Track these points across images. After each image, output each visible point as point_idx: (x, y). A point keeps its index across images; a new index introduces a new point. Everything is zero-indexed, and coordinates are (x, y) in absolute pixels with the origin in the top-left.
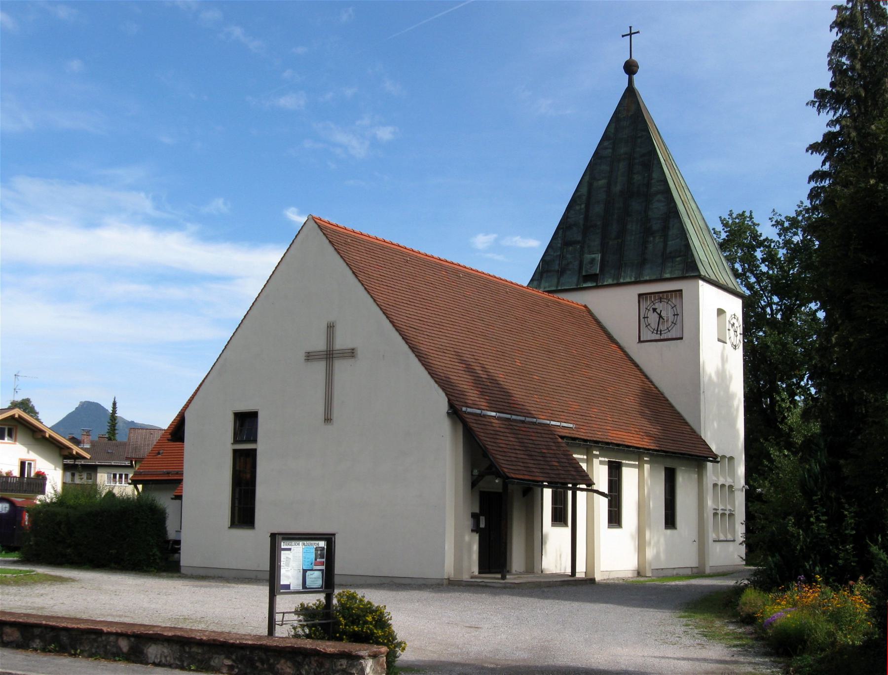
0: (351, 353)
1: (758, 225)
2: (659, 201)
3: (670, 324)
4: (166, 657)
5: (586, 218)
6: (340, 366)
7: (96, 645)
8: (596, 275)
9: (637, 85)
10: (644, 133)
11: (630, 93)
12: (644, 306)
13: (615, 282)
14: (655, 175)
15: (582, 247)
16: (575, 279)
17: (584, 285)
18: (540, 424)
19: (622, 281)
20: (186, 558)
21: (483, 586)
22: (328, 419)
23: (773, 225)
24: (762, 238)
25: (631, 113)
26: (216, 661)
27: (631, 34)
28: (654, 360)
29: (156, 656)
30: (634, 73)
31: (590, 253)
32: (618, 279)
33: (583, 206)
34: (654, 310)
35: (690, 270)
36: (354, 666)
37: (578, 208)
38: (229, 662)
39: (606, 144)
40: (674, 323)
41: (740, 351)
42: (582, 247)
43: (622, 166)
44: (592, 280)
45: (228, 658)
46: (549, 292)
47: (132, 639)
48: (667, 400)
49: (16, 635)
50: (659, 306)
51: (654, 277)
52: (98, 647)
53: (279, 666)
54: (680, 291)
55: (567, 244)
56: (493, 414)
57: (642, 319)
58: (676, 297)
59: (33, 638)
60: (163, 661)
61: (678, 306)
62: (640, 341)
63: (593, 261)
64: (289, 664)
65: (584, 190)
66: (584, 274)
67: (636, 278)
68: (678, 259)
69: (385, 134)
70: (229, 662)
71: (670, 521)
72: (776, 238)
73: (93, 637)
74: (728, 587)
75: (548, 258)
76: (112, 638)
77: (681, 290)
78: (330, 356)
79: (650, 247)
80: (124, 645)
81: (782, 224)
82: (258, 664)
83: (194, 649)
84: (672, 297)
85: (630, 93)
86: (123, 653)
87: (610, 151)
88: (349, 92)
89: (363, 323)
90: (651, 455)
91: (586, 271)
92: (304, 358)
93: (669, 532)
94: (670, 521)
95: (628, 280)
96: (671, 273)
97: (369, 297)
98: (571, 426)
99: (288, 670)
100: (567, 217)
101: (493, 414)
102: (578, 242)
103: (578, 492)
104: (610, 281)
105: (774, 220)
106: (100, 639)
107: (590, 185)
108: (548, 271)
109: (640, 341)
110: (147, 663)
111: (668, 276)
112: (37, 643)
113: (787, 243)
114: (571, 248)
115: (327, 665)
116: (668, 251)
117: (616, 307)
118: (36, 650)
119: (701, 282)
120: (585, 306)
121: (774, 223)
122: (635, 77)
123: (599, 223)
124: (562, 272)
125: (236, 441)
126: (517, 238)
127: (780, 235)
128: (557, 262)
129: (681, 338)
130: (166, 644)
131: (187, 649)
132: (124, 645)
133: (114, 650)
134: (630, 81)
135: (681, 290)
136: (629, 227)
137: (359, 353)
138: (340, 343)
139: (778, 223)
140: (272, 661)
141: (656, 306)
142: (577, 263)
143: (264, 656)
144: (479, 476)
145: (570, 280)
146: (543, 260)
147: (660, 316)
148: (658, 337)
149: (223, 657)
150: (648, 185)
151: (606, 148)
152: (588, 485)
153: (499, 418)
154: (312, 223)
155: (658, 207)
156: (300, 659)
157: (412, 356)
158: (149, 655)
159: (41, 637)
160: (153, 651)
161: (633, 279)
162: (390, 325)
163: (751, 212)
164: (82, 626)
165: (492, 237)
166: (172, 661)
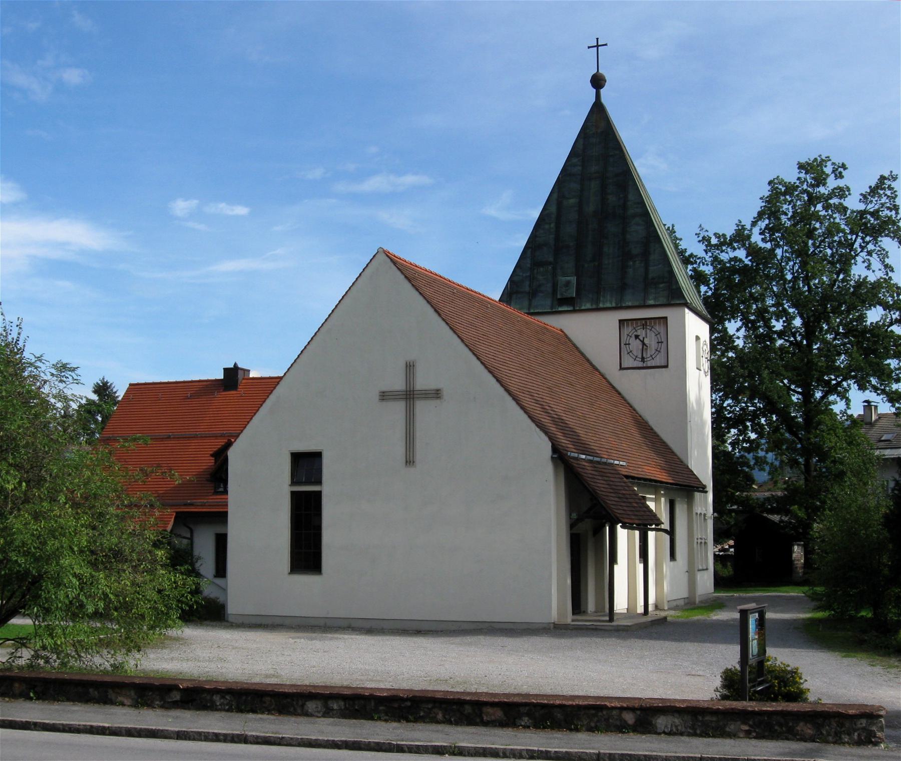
0: (436, 394)
1: (681, 239)
3: (655, 353)
4: (676, 727)
5: (557, 238)
6: (421, 406)
7: (596, 719)
8: (572, 298)
10: (617, 152)
11: (598, 110)
12: (627, 330)
13: (594, 306)
14: (631, 197)
15: (554, 269)
16: (548, 302)
17: (560, 309)
18: (605, 463)
19: (601, 305)
22: (410, 461)
23: (699, 241)
24: (687, 254)
25: (599, 131)
26: (732, 727)
27: (597, 46)
28: (636, 386)
29: (666, 726)
30: (602, 86)
31: (565, 275)
32: (597, 303)
33: (552, 225)
34: (637, 337)
35: (675, 298)
36: (874, 724)
37: (547, 226)
38: (746, 728)
39: (575, 160)
40: (658, 351)
41: (709, 377)
42: (554, 269)
43: (594, 185)
44: (569, 304)
45: (745, 723)
46: (529, 314)
47: (638, 712)
48: (652, 429)
49: (499, 714)
50: (641, 333)
51: (637, 304)
52: (598, 721)
53: (798, 728)
54: (665, 319)
55: (537, 264)
56: (583, 457)
57: (623, 345)
58: (659, 324)
59: (520, 716)
60: (674, 730)
61: (662, 334)
62: (621, 368)
63: (568, 284)
64: (809, 726)
65: (553, 209)
66: (559, 297)
67: (617, 304)
68: (661, 286)
69: (73, 76)
70: (746, 728)
71: (673, 556)
72: (703, 254)
73: (593, 712)
74: (803, 619)
75: (516, 279)
76: (614, 712)
77: (666, 318)
78: (410, 396)
79: (630, 271)
80: (629, 718)
81: (709, 240)
82: (776, 728)
83: (708, 718)
84: (655, 323)
85: (598, 110)
86: (629, 725)
87: (580, 168)
88: (33, 26)
89: (446, 361)
90: (666, 489)
91: (562, 294)
92: (378, 397)
93: (672, 563)
94: (673, 556)
95: (608, 305)
96: (655, 299)
97: (456, 337)
98: (624, 464)
99: (809, 731)
100: (536, 236)
101: (583, 457)
102: (550, 263)
103: (650, 533)
104: (588, 306)
105: (701, 236)
106: (600, 714)
107: (559, 205)
108: (517, 292)
109: (621, 368)
110: (659, 734)
111: (651, 302)
112: (526, 720)
113: (716, 259)
114: (542, 269)
115: (847, 724)
116: (650, 276)
117: (595, 332)
118: (526, 727)
119: (687, 310)
120: (561, 331)
121: (700, 238)
122: (602, 91)
123: (571, 244)
124: (533, 294)
125: (294, 483)
126: (222, 205)
127: (706, 251)
128: (527, 283)
129: (666, 367)
130: (676, 715)
131: (700, 718)
132: (629, 718)
133: (618, 723)
135: (666, 318)
136: (606, 249)
137: (445, 393)
138: (422, 382)
139: (706, 240)
140: (791, 724)
141: (639, 333)
142: (550, 285)
143: (782, 720)
144: (577, 519)
145: (545, 302)
146: (511, 280)
147: (644, 344)
148: (641, 364)
149: (739, 723)
150: (624, 207)
152: (657, 525)
153: (591, 461)
154: (382, 257)
155: (636, 231)
156: (820, 721)
157: (509, 399)
158: (658, 726)
159: (528, 714)
160: (661, 722)
161: (614, 305)
162: (482, 367)
163: (673, 226)
164: (576, 702)
165: (194, 203)
166: (683, 730)
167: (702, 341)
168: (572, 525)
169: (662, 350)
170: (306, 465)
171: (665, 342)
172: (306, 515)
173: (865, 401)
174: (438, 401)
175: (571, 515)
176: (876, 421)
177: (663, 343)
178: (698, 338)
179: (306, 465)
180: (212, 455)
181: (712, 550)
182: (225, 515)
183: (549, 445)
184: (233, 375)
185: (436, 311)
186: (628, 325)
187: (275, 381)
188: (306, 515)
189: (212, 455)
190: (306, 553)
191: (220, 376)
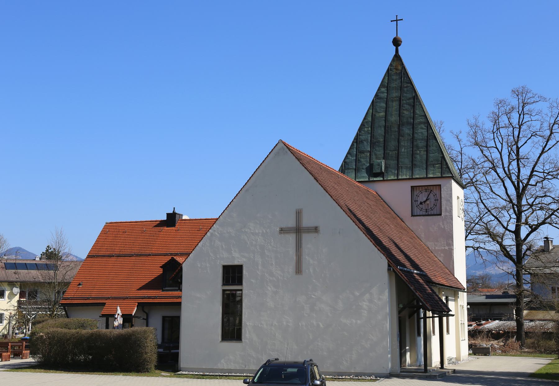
0: (316, 230)
2: (422, 128)
9: (400, 53)
11: (397, 57)
13: (396, 178)
17: (375, 179)
19: (400, 177)
20: (185, 359)
21: (365, 374)
22: (299, 270)
25: (398, 72)
27: (397, 20)
30: (400, 45)
39: (383, 89)
43: (395, 105)
61: (437, 195)
62: (412, 216)
68: (437, 166)
77: (440, 185)
85: (397, 57)
95: (404, 177)
96: (433, 174)
104: (392, 177)
107: (373, 116)
109: (412, 216)
111: (431, 176)
117: (396, 193)
119: (453, 181)
122: (399, 48)
134: (397, 51)
135: (440, 185)
136: (402, 144)
138: (306, 222)
151: (383, 92)
154: (281, 145)
155: (421, 131)
161: (408, 177)
167: (460, 199)
168: (400, 312)
169: (438, 205)
170: (233, 274)
171: (440, 200)
172: (232, 307)
173: (545, 238)
174: (317, 234)
175: (399, 305)
176: (552, 249)
177: (439, 200)
178: (458, 198)
179: (233, 274)
180: (161, 267)
181: (466, 329)
182: (179, 304)
183: (384, 262)
184: (172, 219)
185: (315, 179)
186: (416, 190)
187: (209, 223)
188: (232, 307)
189: (161, 267)
190: (232, 330)
191: (165, 218)
